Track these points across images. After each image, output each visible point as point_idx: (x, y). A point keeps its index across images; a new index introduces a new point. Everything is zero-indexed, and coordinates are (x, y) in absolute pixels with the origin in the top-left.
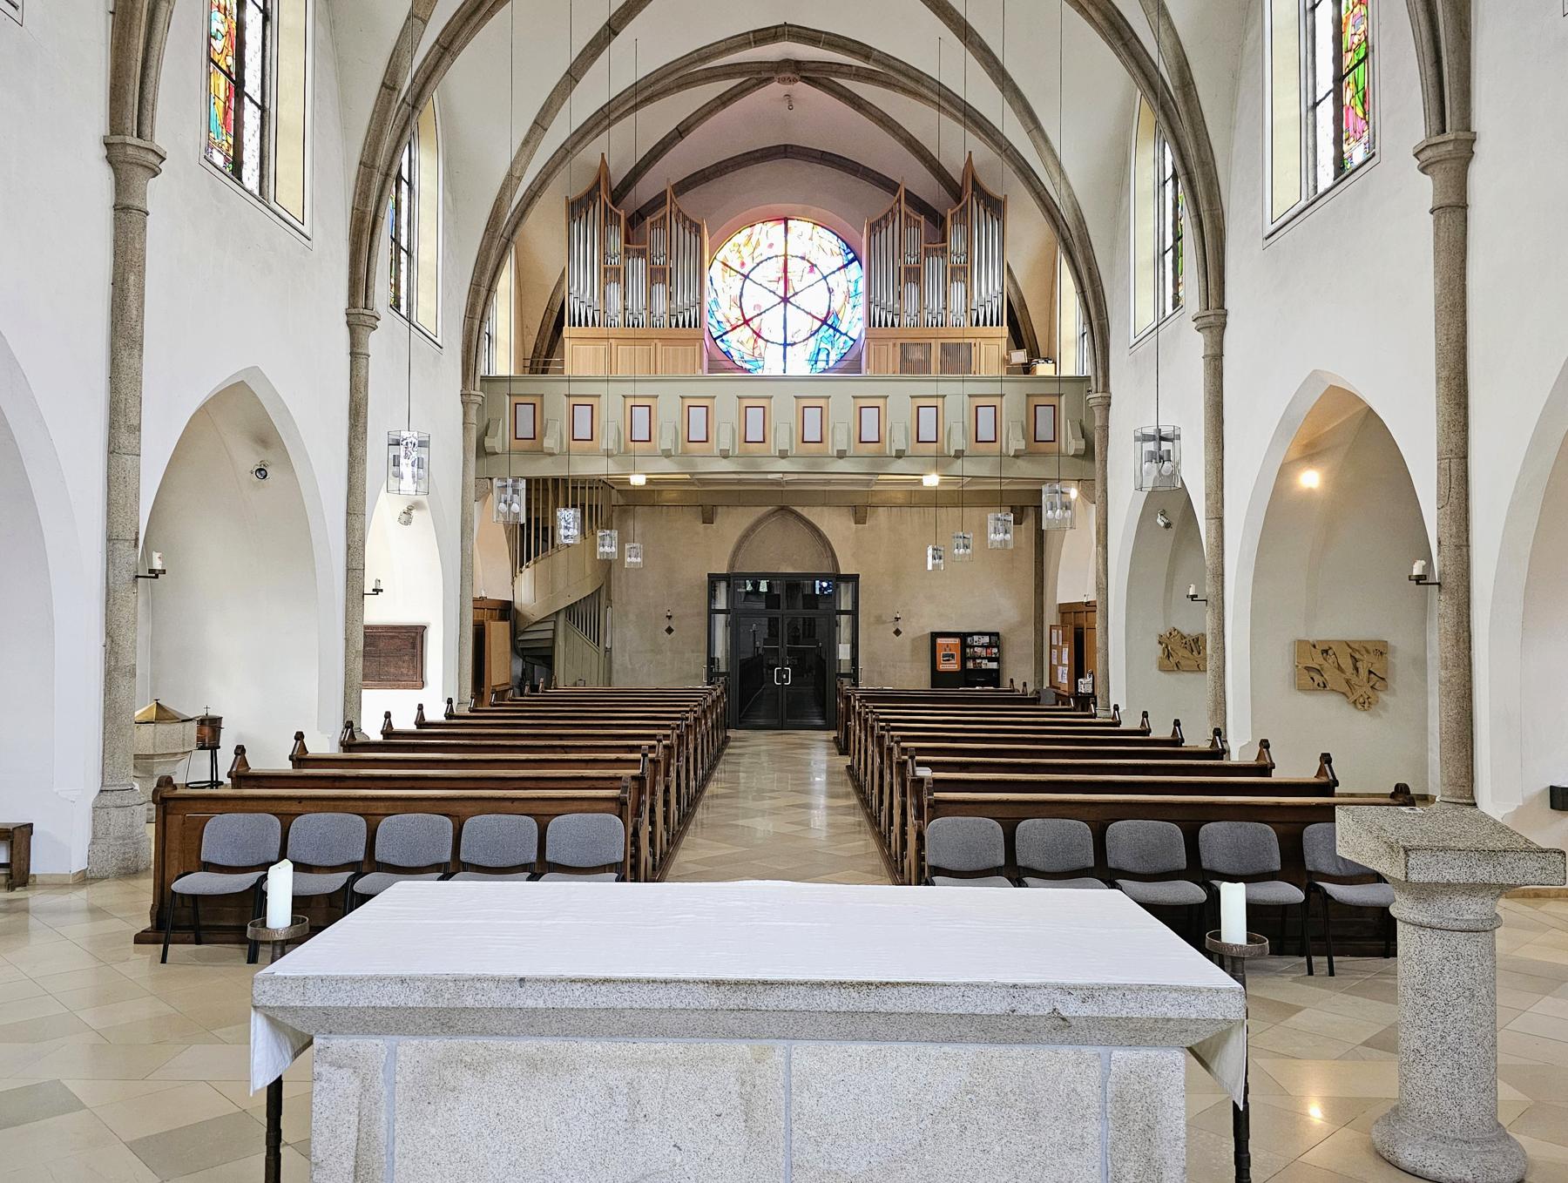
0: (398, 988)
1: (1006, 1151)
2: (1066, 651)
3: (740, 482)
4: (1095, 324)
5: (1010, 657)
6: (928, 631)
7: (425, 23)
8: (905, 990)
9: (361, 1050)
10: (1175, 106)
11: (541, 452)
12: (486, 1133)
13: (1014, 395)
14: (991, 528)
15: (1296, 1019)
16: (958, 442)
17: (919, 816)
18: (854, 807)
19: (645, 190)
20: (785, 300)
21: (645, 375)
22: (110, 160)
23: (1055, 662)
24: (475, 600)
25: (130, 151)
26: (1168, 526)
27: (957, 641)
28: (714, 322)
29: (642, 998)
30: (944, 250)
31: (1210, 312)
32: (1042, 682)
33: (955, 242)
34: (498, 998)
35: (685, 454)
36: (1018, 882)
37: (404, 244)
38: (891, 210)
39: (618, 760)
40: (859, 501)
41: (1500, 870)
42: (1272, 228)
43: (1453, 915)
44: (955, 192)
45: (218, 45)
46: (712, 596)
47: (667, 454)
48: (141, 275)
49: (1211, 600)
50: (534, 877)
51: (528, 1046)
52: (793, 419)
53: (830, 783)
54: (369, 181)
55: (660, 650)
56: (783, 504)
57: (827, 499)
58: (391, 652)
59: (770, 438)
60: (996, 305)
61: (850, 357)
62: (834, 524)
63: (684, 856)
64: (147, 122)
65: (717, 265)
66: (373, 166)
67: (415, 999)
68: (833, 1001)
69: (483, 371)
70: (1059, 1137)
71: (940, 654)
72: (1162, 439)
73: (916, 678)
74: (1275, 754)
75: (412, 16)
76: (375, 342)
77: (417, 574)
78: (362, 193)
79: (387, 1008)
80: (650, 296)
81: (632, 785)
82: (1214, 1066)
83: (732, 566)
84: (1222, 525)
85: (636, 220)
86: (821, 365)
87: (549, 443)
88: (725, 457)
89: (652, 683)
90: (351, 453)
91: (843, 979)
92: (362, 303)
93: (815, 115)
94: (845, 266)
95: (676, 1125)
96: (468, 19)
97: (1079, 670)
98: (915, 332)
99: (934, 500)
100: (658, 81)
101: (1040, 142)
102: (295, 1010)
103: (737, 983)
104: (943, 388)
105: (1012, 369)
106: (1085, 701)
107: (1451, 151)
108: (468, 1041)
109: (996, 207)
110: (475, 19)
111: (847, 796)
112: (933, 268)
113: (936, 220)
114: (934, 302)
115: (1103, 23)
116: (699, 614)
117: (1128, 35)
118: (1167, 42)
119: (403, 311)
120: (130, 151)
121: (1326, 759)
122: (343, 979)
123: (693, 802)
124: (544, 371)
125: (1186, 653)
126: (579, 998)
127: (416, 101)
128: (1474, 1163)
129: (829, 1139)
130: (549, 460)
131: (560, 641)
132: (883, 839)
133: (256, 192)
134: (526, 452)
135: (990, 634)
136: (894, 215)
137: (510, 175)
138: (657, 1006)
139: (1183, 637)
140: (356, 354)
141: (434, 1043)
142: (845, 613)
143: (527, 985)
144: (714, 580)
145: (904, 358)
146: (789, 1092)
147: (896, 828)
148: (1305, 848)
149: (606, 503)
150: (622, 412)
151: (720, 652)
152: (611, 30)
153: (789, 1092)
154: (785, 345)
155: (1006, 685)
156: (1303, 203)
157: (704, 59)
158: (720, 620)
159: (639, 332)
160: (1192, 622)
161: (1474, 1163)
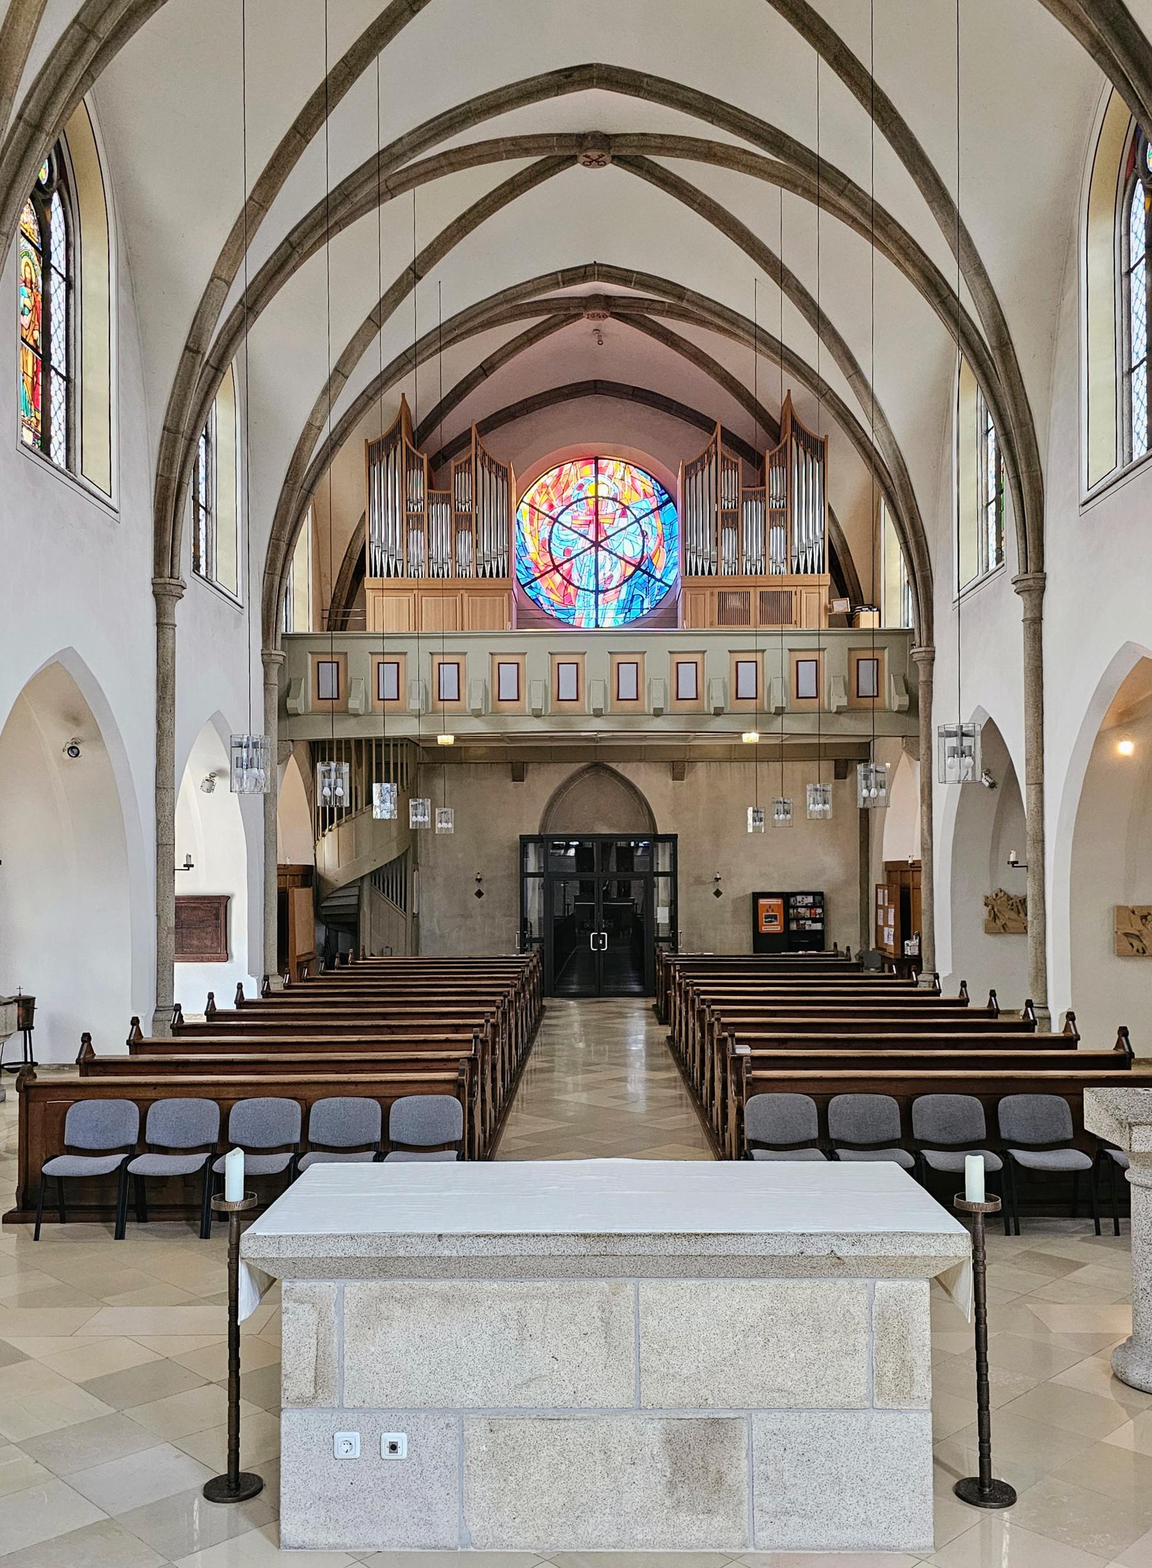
0: (348, 1243)
1: (798, 1356)
2: (892, 912)
3: (551, 739)
4: (918, 575)
6: (750, 891)
8: (723, 1239)
9: (317, 1290)
10: (992, 360)
11: (346, 713)
12: (412, 1350)
13: (836, 648)
14: (810, 800)
15: (1078, 1273)
17: (739, 1092)
18: (675, 1079)
20: (596, 544)
22: (155, 594)
23: (881, 923)
24: (280, 867)
26: (992, 786)
27: (778, 902)
29: (529, 1247)
30: (763, 493)
32: (868, 944)
33: (775, 486)
34: (422, 1249)
35: (496, 713)
36: (832, 1156)
37: (202, 501)
38: (708, 452)
39: (447, 1041)
40: (678, 756)
42: (1087, 495)
44: (773, 429)
46: (524, 854)
49: (1031, 866)
50: (379, 1158)
51: (441, 1285)
52: (606, 673)
53: (650, 1054)
54: (174, 447)
55: (466, 918)
56: (596, 760)
57: (644, 753)
58: (198, 925)
59: (584, 696)
60: (817, 552)
61: (665, 605)
62: (651, 782)
63: (510, 1133)
65: (524, 508)
66: (177, 432)
67: (361, 1251)
68: (670, 1247)
71: (762, 915)
72: (964, 735)
73: (735, 940)
74: (1080, 1026)
76: (181, 611)
79: (340, 1258)
81: (466, 1067)
82: (953, 1293)
83: (543, 826)
84: (1042, 791)
85: (439, 461)
86: (635, 613)
87: (354, 704)
88: (538, 716)
89: (463, 950)
91: (677, 1231)
92: (167, 572)
93: (626, 351)
94: (659, 508)
97: (905, 930)
98: (732, 581)
99: (755, 754)
100: (461, 324)
101: (861, 388)
102: (272, 1260)
103: (599, 1235)
105: (835, 621)
107: (1033, 585)
108: (398, 1283)
109: (817, 449)
111: (668, 1068)
112: (752, 514)
114: (753, 548)
115: (922, 281)
116: (510, 876)
117: (945, 293)
118: (985, 301)
121: (1123, 1032)
122: (308, 1237)
123: (516, 1077)
124: (343, 626)
125: (1010, 914)
126: (483, 1248)
127: (218, 368)
129: (668, 1351)
130: (353, 721)
131: (365, 908)
132: (704, 1112)
133: (63, 466)
134: (324, 713)
135: (814, 894)
136: (710, 457)
137: (310, 424)
138: (541, 1253)
139: (1009, 898)
140: (163, 623)
141: (372, 1284)
143: (444, 1240)
144: (525, 840)
145: (722, 608)
147: (717, 1101)
149: (411, 763)
150: (433, 667)
152: (415, 273)
155: (829, 950)
156: (1119, 471)
160: (1020, 885)
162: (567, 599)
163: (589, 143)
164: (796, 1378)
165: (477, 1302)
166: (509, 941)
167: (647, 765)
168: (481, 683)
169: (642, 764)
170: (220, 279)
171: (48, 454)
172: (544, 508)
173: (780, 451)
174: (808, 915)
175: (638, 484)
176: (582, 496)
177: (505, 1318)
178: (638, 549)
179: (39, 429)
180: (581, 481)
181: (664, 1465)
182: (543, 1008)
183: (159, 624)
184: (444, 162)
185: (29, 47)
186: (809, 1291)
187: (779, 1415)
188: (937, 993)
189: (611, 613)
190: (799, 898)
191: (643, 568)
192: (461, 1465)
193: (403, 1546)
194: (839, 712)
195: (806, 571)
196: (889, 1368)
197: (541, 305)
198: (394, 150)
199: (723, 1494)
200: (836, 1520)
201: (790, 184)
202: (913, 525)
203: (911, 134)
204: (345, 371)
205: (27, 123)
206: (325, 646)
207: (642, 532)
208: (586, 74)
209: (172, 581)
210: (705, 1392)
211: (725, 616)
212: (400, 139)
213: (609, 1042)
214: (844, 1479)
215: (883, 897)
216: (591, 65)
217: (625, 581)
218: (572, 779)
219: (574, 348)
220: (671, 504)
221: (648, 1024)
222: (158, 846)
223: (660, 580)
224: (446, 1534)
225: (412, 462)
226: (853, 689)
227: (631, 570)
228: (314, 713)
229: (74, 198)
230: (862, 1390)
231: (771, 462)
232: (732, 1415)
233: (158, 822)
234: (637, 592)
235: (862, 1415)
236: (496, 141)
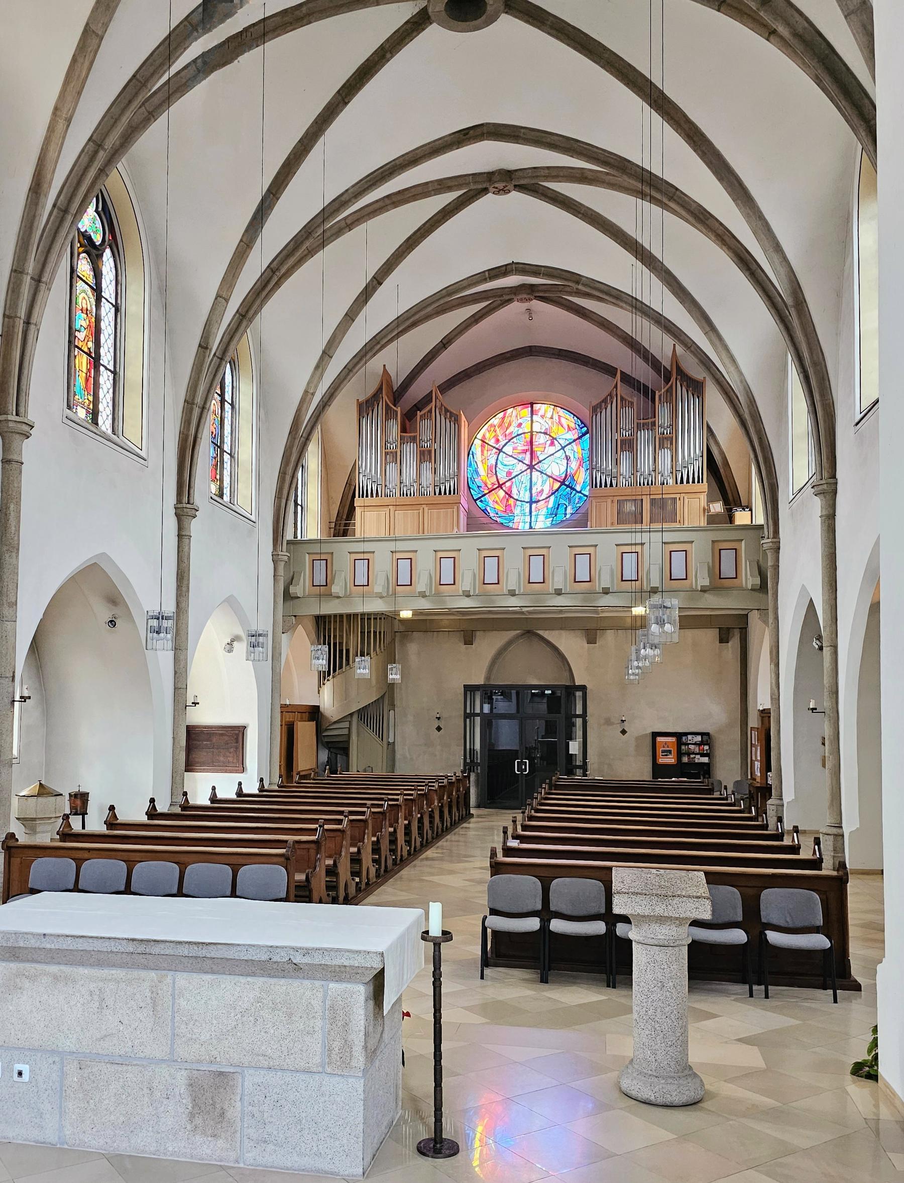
3: (431, 614)
4: (766, 482)
7: (227, 301)
8: (219, 946)
11: (330, 595)
19: (417, 391)
21: (415, 535)
24: (283, 706)
25: (11, 424)
27: (673, 739)
30: (654, 424)
31: (823, 482)
33: (663, 416)
34: (33, 943)
35: (438, 594)
38: (610, 395)
41: (670, 908)
43: (652, 936)
45: (81, 335)
47: (423, 595)
48: (18, 504)
49: (827, 711)
51: (54, 969)
55: (428, 748)
56: (528, 628)
57: (564, 623)
58: (204, 745)
60: (699, 465)
61: (582, 511)
62: (570, 644)
64: (22, 404)
65: (478, 443)
66: (193, 404)
68: (185, 951)
69: (289, 536)
70: (302, 1027)
73: (637, 769)
75: (218, 296)
76: (195, 527)
77: (231, 689)
80: (419, 475)
83: (488, 678)
86: (561, 517)
87: (336, 589)
88: (468, 596)
92: (185, 499)
93: (551, 323)
94: (580, 438)
95: (121, 1011)
96: (258, 294)
97: (767, 767)
103: (142, 940)
105: (712, 519)
109: (696, 388)
110: (264, 293)
114: (645, 462)
117: (754, 267)
118: (782, 271)
119: (226, 498)
120: (11, 424)
124: (345, 534)
128: (656, 1089)
130: (337, 601)
131: (354, 737)
133: (110, 432)
134: (315, 596)
135: (702, 734)
136: (612, 398)
137: (306, 392)
140: (182, 536)
142: (579, 716)
144: (469, 689)
146: (174, 998)
148: (762, 906)
149: (382, 634)
150: (402, 560)
152: (378, 280)
153: (174, 998)
154: (531, 502)
157: (449, 295)
158: (579, 711)
161: (656, 1089)
162: (508, 509)
163: (495, 178)
164: (275, 1047)
165: (74, 981)
167: (568, 632)
168: (427, 573)
169: (562, 632)
170: (222, 298)
171: (97, 424)
172: (492, 442)
173: (667, 391)
174: (697, 750)
175: (563, 421)
176: (520, 431)
177: (91, 994)
178: (563, 469)
179: (91, 407)
180: (520, 421)
181: (187, 1101)
183: (180, 536)
184: (388, 201)
185: (57, 162)
186: (284, 988)
187: (262, 1073)
189: (541, 518)
190: (690, 737)
191: (567, 483)
192: (61, 1089)
193: (25, 1140)
194: (704, 590)
195: (688, 482)
196: (337, 1045)
197: (488, 292)
198: (343, 199)
199: (224, 1124)
200: (297, 1149)
201: (642, 195)
203: (718, 151)
205: (60, 209)
206: (326, 548)
207: (566, 456)
208: (479, 131)
209: (188, 506)
210: (215, 1053)
211: (621, 518)
212: (347, 191)
214: (304, 1121)
216: (482, 125)
217: (553, 494)
218: (510, 643)
219: (513, 323)
223: (580, 492)
224: (50, 1135)
225: (389, 414)
226: (716, 573)
227: (557, 485)
228: (309, 596)
230: (317, 1059)
231: (660, 399)
232: (232, 1070)
233: (176, 673)
234: (562, 501)
235: (317, 1077)
236: (427, 183)
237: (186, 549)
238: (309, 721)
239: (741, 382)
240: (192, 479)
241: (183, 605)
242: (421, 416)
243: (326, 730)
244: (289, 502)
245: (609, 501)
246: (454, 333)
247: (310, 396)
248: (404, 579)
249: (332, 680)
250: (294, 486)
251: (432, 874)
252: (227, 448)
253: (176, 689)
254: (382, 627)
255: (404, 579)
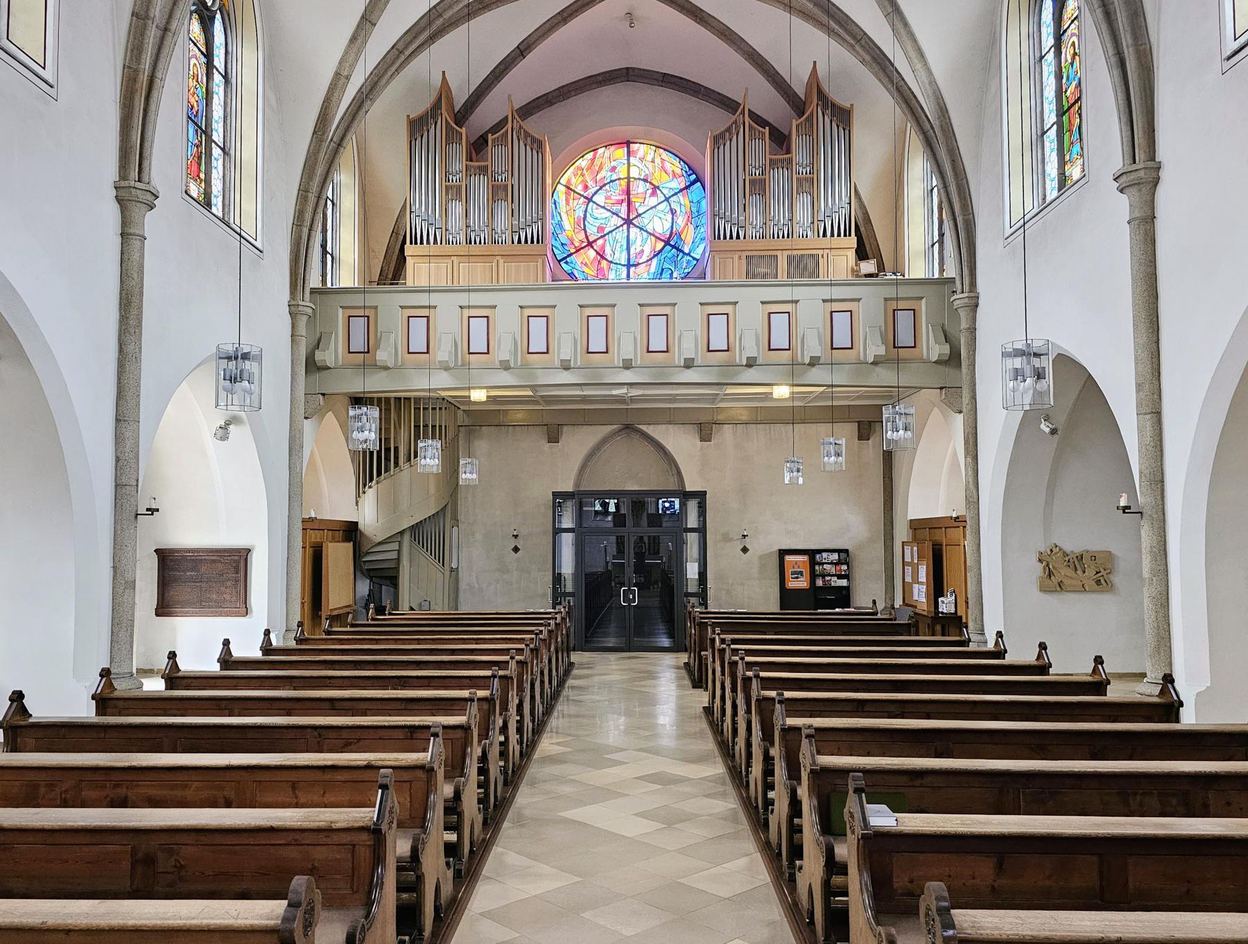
3: (584, 399)
5: (859, 574)
6: (776, 548)
13: (870, 302)
16: (814, 347)
22: (118, 199)
23: (908, 579)
24: (304, 521)
26: (1054, 432)
27: (805, 558)
28: (558, 244)
30: (790, 161)
33: (799, 154)
35: (525, 366)
37: (329, 250)
40: (702, 420)
46: (556, 517)
47: (505, 366)
52: (636, 325)
54: (143, 34)
55: (506, 567)
56: (628, 422)
58: (197, 578)
59: (614, 348)
62: (680, 443)
65: (561, 189)
66: (147, 17)
69: (314, 281)
73: (760, 597)
74: (1052, 655)
76: (152, 223)
78: (135, 49)
83: (577, 484)
85: (478, 146)
87: (382, 356)
88: (567, 368)
90: (121, 350)
94: (687, 187)
97: (938, 590)
98: (762, 244)
101: (899, 26)
104: (797, 293)
106: (955, 622)
107: (1142, 175)
109: (843, 116)
112: (777, 179)
113: (780, 140)
114: (779, 214)
119: (217, 209)
120: (301, 308)
121: (1043, 646)
130: (384, 373)
131: (405, 562)
133: (220, 215)
134: (357, 366)
135: (839, 551)
139: (1065, 554)
140: (128, 235)
144: (560, 498)
149: (458, 423)
150: (471, 326)
151: (567, 567)
154: (629, 266)
156: (1036, 210)
159: (474, 249)
166: (544, 595)
172: (579, 189)
175: (668, 166)
178: (668, 225)
180: (613, 164)
182: (571, 665)
188: (1000, 654)
190: (825, 555)
194: (874, 363)
202: (954, 169)
204: (373, 18)
206: (371, 300)
209: (138, 185)
213: (640, 700)
215: (911, 553)
218: (604, 441)
220: (699, 184)
221: (680, 687)
222: (116, 486)
223: (689, 254)
225: (451, 137)
227: (660, 245)
228: (344, 367)
229: (239, 25)
231: (797, 131)
233: (118, 459)
237: (136, 256)
238: (344, 541)
239: (930, 83)
240: (147, 144)
241: (130, 348)
242: (493, 140)
243: (368, 553)
244: (313, 233)
245: (736, 257)
246: (535, 37)
247: (343, 80)
248: (478, 344)
249: (375, 487)
250: (320, 210)
251: (579, 802)
252: (217, 136)
253: (118, 486)
254: (441, 418)
255: (478, 344)
